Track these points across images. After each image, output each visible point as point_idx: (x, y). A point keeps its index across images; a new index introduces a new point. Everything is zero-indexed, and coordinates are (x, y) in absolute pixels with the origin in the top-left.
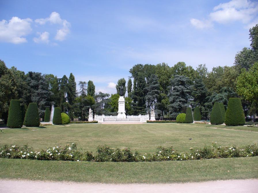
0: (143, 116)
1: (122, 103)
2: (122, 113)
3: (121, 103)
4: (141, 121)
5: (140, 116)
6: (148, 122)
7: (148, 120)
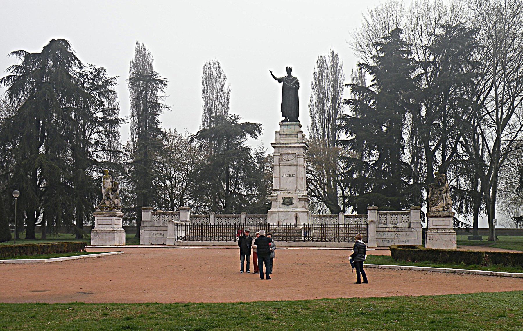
1: (290, 151)
2: (288, 202)
3: (285, 150)
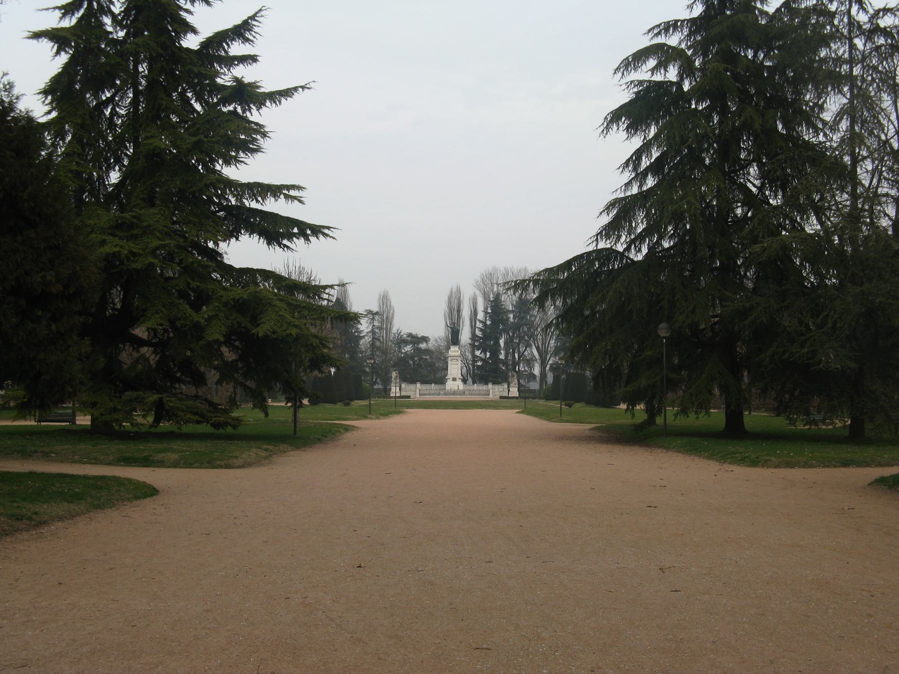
0: (496, 387)
2: (454, 379)
4: (491, 396)
5: (490, 386)
6: (501, 397)
7: (505, 394)
